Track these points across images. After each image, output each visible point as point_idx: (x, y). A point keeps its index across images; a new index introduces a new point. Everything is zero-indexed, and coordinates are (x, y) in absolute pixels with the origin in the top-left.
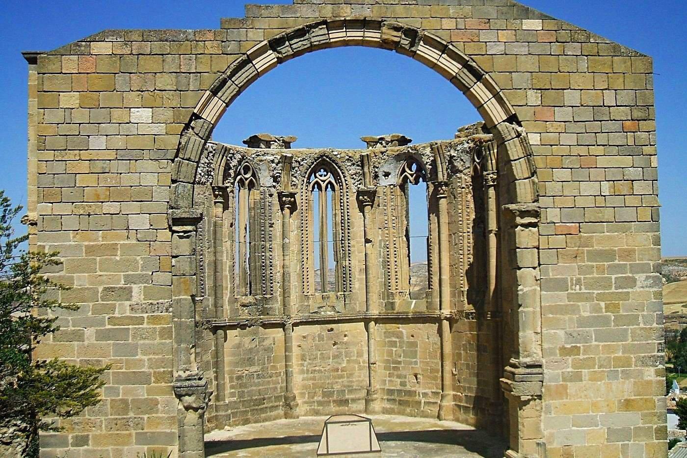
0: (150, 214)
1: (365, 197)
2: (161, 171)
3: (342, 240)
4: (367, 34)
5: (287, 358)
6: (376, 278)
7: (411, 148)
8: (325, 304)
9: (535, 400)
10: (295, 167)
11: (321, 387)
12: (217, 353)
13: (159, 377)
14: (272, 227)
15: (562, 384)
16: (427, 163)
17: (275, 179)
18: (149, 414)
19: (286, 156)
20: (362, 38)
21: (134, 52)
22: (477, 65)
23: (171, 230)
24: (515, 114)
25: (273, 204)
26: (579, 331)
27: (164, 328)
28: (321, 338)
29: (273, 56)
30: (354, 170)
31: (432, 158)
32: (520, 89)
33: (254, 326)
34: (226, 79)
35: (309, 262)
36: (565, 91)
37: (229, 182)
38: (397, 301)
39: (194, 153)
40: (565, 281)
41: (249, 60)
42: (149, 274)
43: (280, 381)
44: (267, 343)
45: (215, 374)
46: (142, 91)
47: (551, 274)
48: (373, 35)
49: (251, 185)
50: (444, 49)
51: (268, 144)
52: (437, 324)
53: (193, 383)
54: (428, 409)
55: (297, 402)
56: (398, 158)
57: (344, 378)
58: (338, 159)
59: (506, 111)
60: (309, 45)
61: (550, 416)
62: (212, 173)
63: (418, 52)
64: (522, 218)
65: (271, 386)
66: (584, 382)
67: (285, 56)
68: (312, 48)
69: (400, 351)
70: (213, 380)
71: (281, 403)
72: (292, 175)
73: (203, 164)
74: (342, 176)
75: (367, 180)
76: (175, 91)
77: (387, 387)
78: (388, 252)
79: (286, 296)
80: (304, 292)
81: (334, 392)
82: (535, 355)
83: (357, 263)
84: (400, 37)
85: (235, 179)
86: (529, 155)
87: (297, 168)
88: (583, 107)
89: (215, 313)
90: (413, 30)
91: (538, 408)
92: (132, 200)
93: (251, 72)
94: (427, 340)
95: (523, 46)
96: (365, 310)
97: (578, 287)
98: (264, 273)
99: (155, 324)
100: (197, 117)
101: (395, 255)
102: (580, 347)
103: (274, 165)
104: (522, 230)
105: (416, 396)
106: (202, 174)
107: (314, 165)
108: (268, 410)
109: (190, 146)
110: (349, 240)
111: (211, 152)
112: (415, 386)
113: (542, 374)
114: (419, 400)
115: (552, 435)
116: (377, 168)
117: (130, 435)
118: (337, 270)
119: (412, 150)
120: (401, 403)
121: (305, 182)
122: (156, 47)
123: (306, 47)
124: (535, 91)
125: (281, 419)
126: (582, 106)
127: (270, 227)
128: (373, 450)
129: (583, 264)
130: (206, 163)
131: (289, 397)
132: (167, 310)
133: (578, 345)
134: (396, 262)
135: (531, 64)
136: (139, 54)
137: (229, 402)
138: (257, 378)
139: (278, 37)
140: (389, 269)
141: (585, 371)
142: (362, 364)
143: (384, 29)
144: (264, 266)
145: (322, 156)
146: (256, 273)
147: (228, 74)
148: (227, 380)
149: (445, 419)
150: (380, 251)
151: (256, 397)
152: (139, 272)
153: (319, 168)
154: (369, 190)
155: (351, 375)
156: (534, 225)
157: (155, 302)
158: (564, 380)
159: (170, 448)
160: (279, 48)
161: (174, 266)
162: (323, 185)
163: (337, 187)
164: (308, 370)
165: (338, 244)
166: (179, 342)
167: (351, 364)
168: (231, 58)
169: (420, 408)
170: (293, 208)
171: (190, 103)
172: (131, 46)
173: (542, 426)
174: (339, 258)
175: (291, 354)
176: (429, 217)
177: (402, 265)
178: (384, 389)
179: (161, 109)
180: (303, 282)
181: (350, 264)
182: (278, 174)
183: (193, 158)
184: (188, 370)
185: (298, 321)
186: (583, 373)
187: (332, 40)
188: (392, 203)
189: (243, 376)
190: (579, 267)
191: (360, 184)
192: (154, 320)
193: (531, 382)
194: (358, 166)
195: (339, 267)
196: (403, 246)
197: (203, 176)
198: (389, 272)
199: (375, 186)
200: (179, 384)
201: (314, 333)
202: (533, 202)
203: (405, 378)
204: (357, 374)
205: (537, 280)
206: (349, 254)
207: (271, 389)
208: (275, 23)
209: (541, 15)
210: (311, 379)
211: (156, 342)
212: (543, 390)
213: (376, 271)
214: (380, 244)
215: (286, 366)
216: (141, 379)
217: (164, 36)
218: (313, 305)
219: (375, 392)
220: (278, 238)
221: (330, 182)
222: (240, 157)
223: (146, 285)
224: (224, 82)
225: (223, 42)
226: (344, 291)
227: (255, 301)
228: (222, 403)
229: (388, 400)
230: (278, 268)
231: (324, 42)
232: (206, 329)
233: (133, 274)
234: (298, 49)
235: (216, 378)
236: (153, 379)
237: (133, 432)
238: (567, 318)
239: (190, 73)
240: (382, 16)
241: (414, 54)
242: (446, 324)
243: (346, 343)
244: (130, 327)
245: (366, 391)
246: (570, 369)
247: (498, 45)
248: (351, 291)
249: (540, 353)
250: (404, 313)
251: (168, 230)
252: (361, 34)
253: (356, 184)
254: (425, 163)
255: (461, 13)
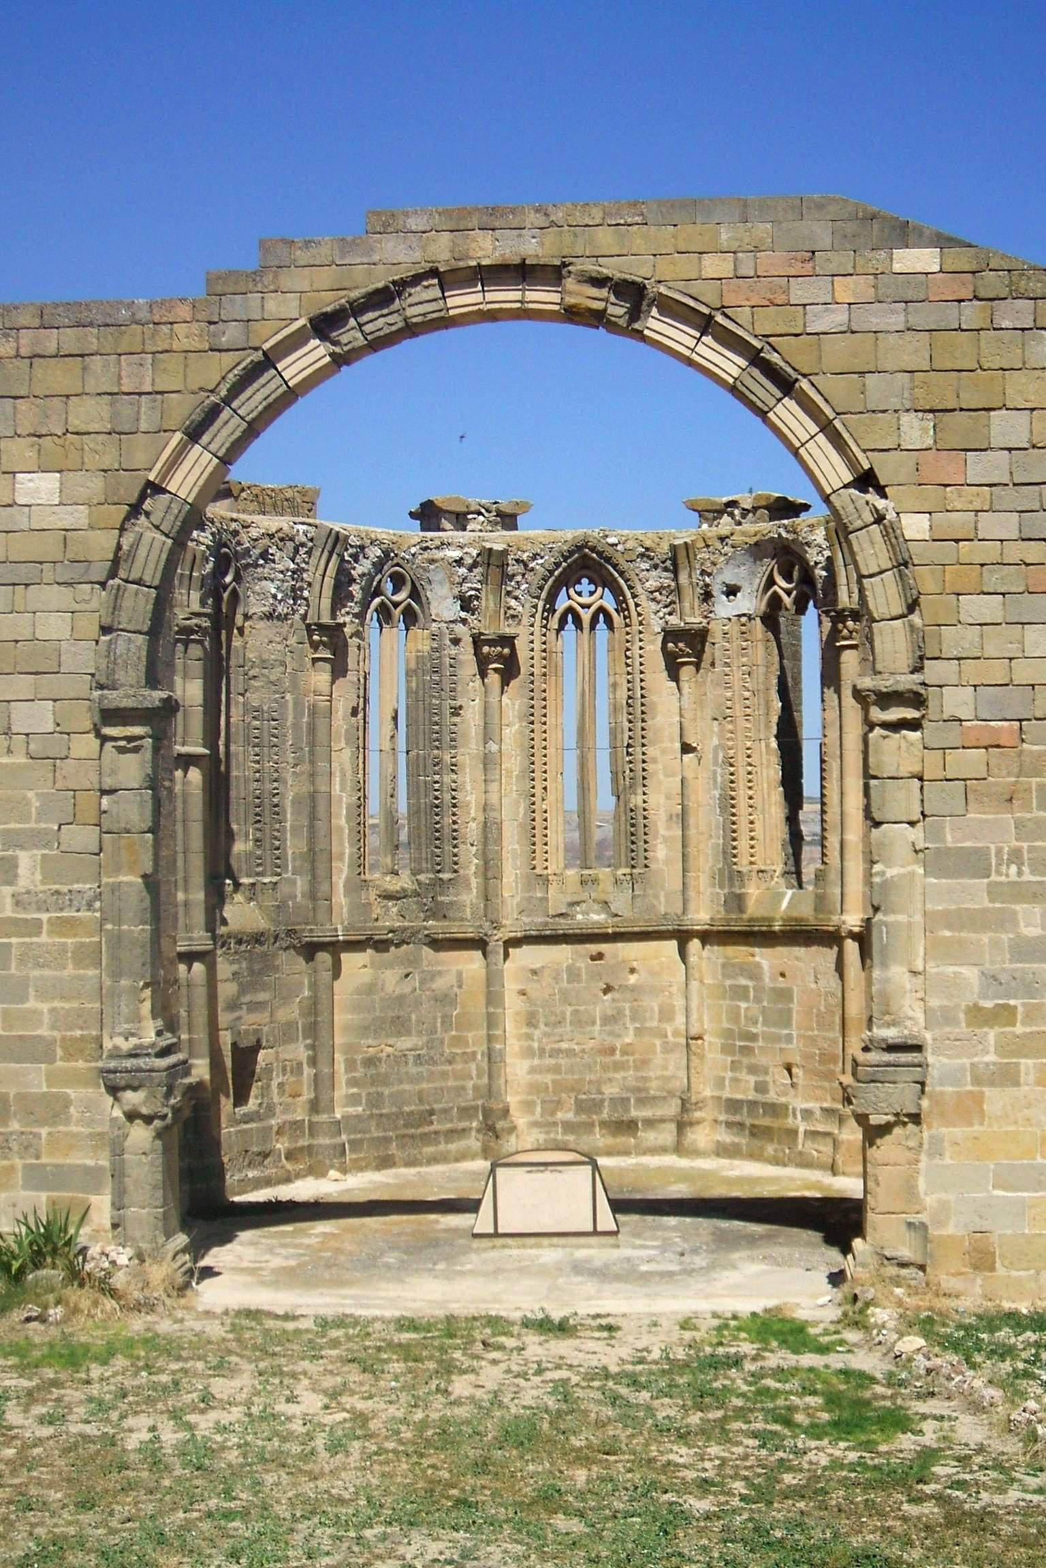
0: (55, 700)
1: (681, 645)
2: (77, 607)
3: (629, 746)
4: (531, 296)
5: (492, 1021)
6: (706, 836)
7: (785, 527)
8: (585, 896)
9: (905, 1124)
10: (514, 575)
11: (573, 1090)
12: (315, 1004)
13: (73, 1049)
14: (458, 715)
15: (971, 1092)
16: (816, 563)
17: (466, 604)
18: (51, 1125)
19: (490, 550)
20: (518, 305)
21: (23, 352)
22: (783, 359)
23: (98, 734)
24: (871, 469)
25: (461, 662)
26: (1015, 970)
27: (82, 945)
28: (573, 974)
29: (322, 351)
30: (655, 579)
31: (827, 553)
32: (884, 411)
33: (408, 943)
34: (217, 404)
35: (551, 797)
36: (992, 413)
37: (348, 613)
38: (753, 891)
39: (151, 565)
40: (982, 853)
41: (268, 362)
42: (52, 830)
43: (474, 1073)
44: (439, 984)
45: (310, 1053)
46: (39, 436)
47: (949, 838)
48: (542, 297)
49: (410, 618)
50: (705, 325)
51: (460, 520)
52: (836, 949)
53: (141, 1062)
54: (811, 1149)
55: (512, 1122)
56: (758, 550)
57: (628, 1069)
58: (618, 555)
59: (852, 462)
60: (401, 324)
61: (941, 1162)
62: (306, 593)
63: (646, 332)
64: (883, 708)
65: (449, 1084)
66: (1025, 1088)
67: (349, 351)
68: (410, 330)
69: (755, 1009)
70: (305, 1066)
71: (474, 1124)
72: (508, 593)
73: (282, 572)
74: (628, 595)
75: (687, 604)
76: (110, 433)
77: (727, 1094)
78: (732, 774)
79: (490, 875)
80: (534, 868)
81: (602, 1101)
82: (908, 1023)
83: (662, 800)
84: (606, 300)
85: (365, 605)
86: (903, 564)
87: (519, 578)
88: (1036, 451)
89: (311, 914)
90: (633, 283)
91: (911, 1143)
92: (18, 669)
93: (274, 387)
94: (813, 986)
95: (893, 312)
96: (680, 912)
97: (1014, 868)
98: (437, 823)
99: (65, 936)
100: (155, 488)
101: (750, 781)
102: (1015, 1007)
103: (463, 571)
104: (884, 738)
105: (786, 1116)
106: (280, 596)
107: (560, 570)
108: (442, 1138)
109: (142, 552)
110: (643, 745)
111: (303, 545)
112: (785, 1094)
113: (920, 1066)
114: (794, 1127)
115: (944, 1206)
116: (709, 575)
117: (12, 1168)
118: (617, 817)
119: (788, 532)
120: (756, 1132)
121: (540, 609)
122: (69, 339)
123: (394, 328)
124: (920, 414)
125: (473, 1159)
126: (1034, 447)
127: (453, 714)
128: (599, 1229)
129: (1028, 816)
130: (288, 570)
131: (491, 1110)
132: (90, 906)
133: (1012, 1002)
134: (751, 798)
135: (913, 352)
136: (35, 356)
137: (343, 1117)
138: (416, 1064)
139: (329, 309)
140: (734, 815)
141: (1026, 1064)
142: (671, 1038)
143: (570, 283)
144: (437, 807)
145: (579, 548)
146: (419, 821)
147: (223, 393)
148: (340, 1066)
149: (844, 1174)
150: (715, 773)
151: (413, 1108)
152: (32, 825)
153: (577, 575)
154: (687, 627)
155: (644, 1063)
156: (914, 725)
157: (65, 889)
158: (977, 1081)
159: (94, 1199)
160: (334, 334)
161: (105, 812)
162: (586, 616)
163: (617, 620)
164: (542, 1051)
165: (620, 755)
166: (116, 975)
167: (646, 1039)
168: (228, 359)
169: (796, 1145)
170: (510, 670)
171: (139, 460)
172: (17, 339)
173: (922, 1184)
174: (621, 788)
175: (501, 1010)
176: (823, 693)
177: (767, 807)
178: (719, 1098)
179: (80, 473)
180: (534, 844)
181: (645, 802)
182: (473, 593)
183: (147, 579)
184: (133, 1035)
185: (519, 935)
186: (1022, 1068)
187: (451, 312)
188: (744, 659)
189: (380, 1060)
190: (1019, 825)
191: (670, 614)
192: (63, 926)
193: (894, 1083)
194: (666, 569)
195: (622, 809)
196: (769, 760)
197: (280, 601)
198: (734, 823)
199: (706, 617)
200: (112, 1064)
201: (558, 964)
202: (912, 673)
203: (766, 1073)
204: (658, 1059)
205: (916, 852)
206: (644, 778)
207: (450, 1089)
208: (325, 277)
209: (939, 236)
210: (549, 1070)
211: (66, 973)
212: (925, 1103)
213: (706, 818)
214: (716, 756)
215: (490, 1039)
216: (36, 1051)
217: (84, 316)
218: (557, 899)
219: (700, 1105)
220: (473, 741)
221: (601, 609)
222: (379, 553)
223: (46, 852)
224: (213, 413)
225: (210, 323)
226: (633, 867)
227: (416, 886)
228: (324, 1117)
229: (729, 1125)
230: (473, 812)
231: (435, 315)
232: (287, 948)
233: (20, 829)
234: (378, 334)
235: (313, 1061)
236: (60, 1052)
237: (18, 1162)
238: (986, 940)
239: (140, 394)
240: (564, 254)
241: (639, 336)
242: (851, 947)
243: (633, 989)
244: (14, 940)
245: (679, 1102)
246: (991, 1058)
247: (833, 311)
248: (646, 866)
249: (920, 1017)
250: (764, 919)
251: (92, 736)
252: (516, 295)
253: (661, 614)
254: (812, 563)
255: (746, 241)
